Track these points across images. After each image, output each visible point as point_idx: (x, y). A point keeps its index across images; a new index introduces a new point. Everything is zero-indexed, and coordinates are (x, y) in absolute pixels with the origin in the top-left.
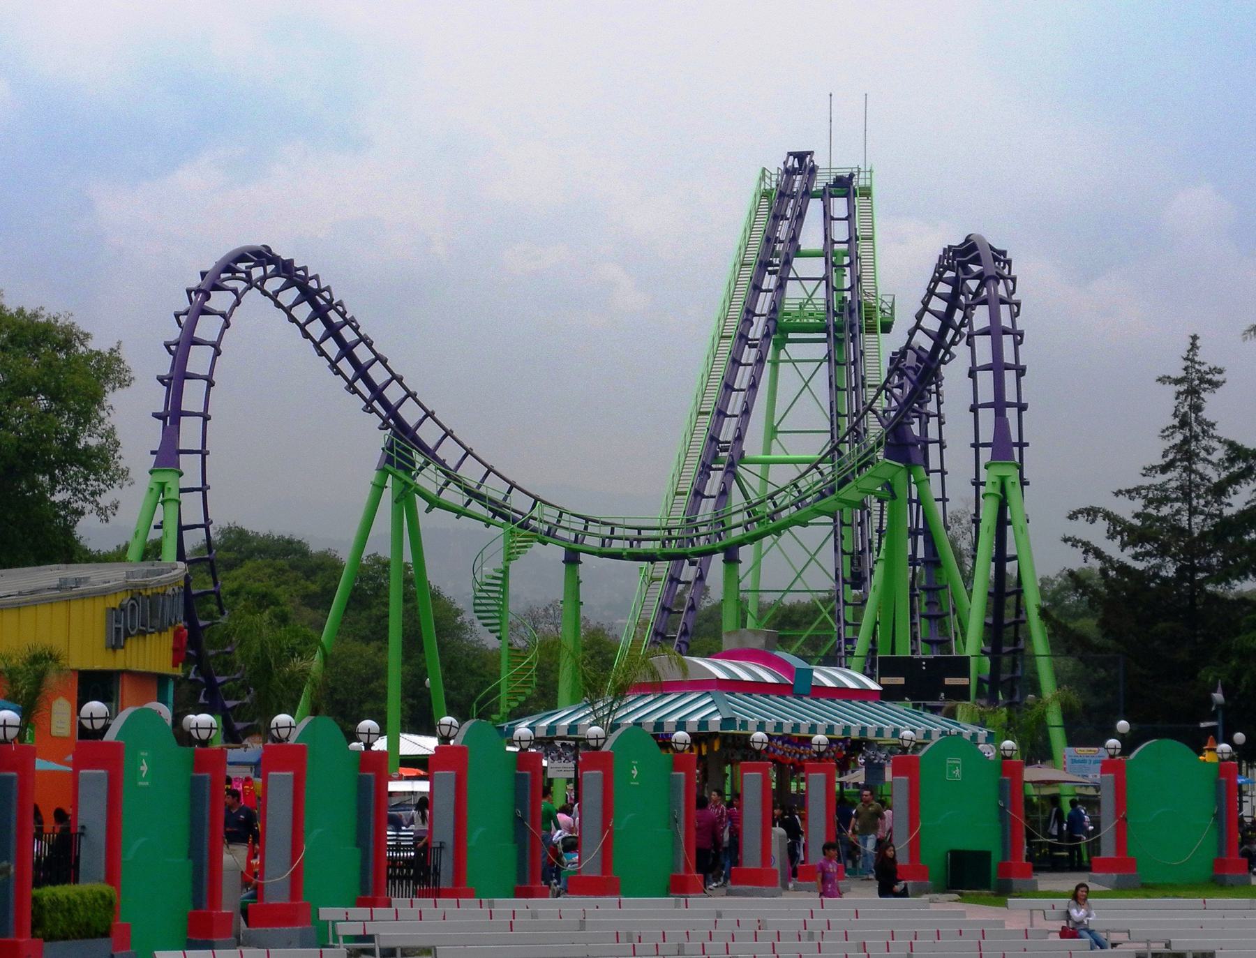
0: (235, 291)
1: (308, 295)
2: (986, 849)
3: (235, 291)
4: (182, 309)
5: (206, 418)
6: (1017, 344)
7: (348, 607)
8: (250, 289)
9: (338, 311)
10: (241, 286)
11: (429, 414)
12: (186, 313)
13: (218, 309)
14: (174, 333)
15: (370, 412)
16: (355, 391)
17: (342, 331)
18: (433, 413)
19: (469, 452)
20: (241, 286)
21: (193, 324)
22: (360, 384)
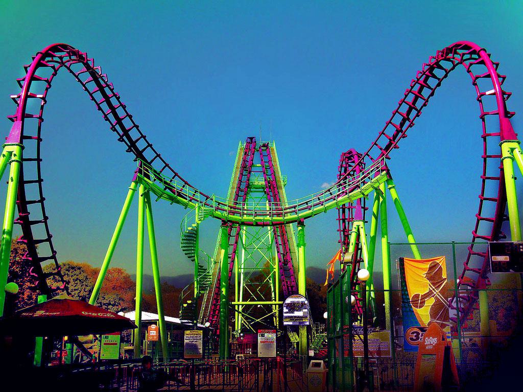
0: (53, 67)
1: (95, 77)
2: (188, 273)
3: (53, 67)
4: (22, 77)
5: (39, 140)
6: (410, 126)
7: (275, 258)
8: (62, 66)
9: (109, 88)
10: (57, 65)
11: (150, 145)
12: (24, 80)
13: (43, 77)
14: (124, 147)
15: (121, 141)
16: (115, 130)
17: (388, 289)
18: (152, 145)
19: (167, 165)
20: (57, 65)
21: (136, 149)
22: (118, 127)
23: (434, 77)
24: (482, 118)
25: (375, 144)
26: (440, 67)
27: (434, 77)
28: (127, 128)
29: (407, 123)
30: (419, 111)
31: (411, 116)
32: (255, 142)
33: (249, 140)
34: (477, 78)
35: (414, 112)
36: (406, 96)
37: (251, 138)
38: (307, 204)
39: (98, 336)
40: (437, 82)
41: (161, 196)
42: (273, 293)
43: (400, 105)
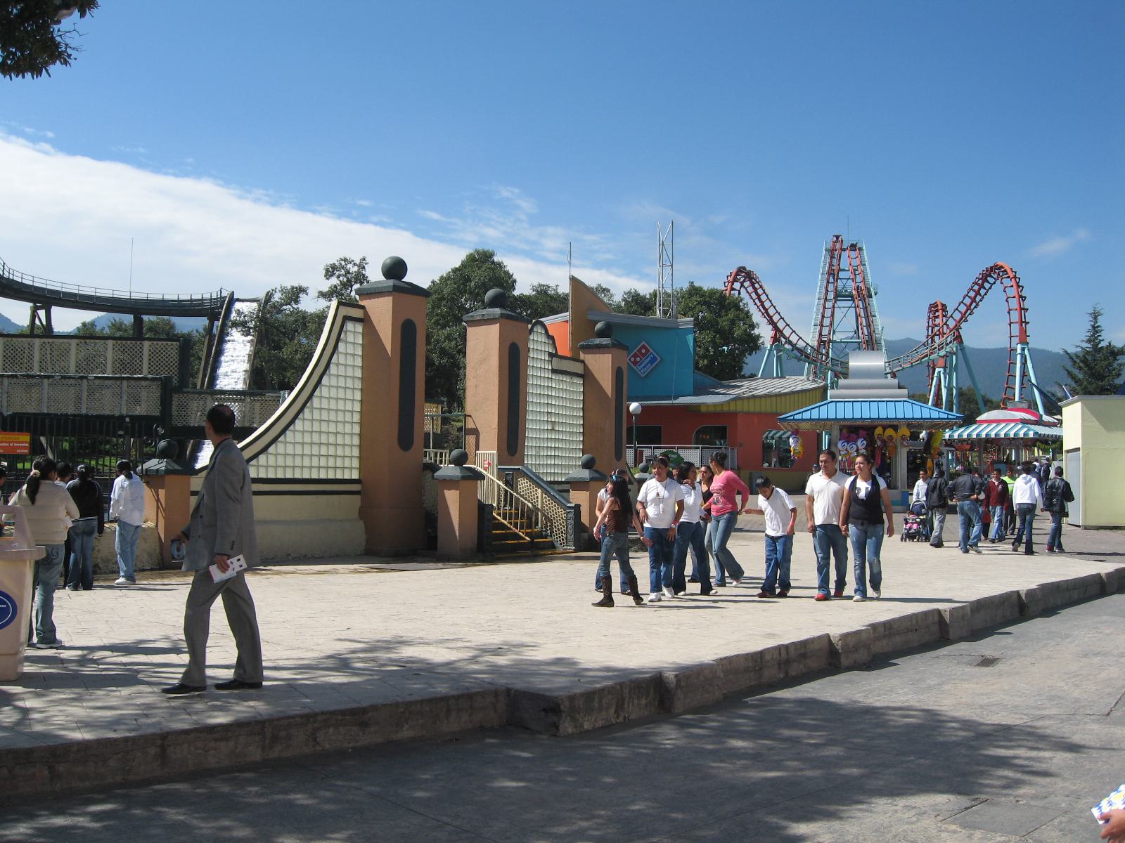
23: (988, 282)
24: (1009, 312)
25: (1010, 310)
26: (992, 277)
27: (988, 282)
28: (767, 307)
29: (969, 312)
30: (977, 304)
31: (972, 307)
32: (842, 241)
33: (835, 239)
34: (1006, 287)
35: (974, 304)
36: (968, 292)
37: (837, 237)
38: (834, 258)
39: (722, 441)
40: (989, 285)
41: (1024, 309)
42: (667, 746)
43: (964, 298)
